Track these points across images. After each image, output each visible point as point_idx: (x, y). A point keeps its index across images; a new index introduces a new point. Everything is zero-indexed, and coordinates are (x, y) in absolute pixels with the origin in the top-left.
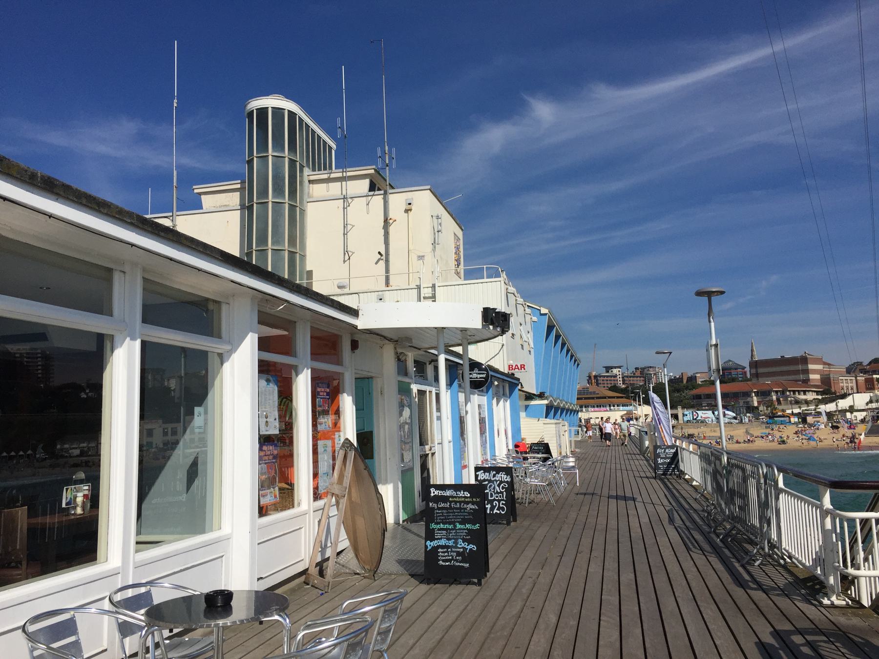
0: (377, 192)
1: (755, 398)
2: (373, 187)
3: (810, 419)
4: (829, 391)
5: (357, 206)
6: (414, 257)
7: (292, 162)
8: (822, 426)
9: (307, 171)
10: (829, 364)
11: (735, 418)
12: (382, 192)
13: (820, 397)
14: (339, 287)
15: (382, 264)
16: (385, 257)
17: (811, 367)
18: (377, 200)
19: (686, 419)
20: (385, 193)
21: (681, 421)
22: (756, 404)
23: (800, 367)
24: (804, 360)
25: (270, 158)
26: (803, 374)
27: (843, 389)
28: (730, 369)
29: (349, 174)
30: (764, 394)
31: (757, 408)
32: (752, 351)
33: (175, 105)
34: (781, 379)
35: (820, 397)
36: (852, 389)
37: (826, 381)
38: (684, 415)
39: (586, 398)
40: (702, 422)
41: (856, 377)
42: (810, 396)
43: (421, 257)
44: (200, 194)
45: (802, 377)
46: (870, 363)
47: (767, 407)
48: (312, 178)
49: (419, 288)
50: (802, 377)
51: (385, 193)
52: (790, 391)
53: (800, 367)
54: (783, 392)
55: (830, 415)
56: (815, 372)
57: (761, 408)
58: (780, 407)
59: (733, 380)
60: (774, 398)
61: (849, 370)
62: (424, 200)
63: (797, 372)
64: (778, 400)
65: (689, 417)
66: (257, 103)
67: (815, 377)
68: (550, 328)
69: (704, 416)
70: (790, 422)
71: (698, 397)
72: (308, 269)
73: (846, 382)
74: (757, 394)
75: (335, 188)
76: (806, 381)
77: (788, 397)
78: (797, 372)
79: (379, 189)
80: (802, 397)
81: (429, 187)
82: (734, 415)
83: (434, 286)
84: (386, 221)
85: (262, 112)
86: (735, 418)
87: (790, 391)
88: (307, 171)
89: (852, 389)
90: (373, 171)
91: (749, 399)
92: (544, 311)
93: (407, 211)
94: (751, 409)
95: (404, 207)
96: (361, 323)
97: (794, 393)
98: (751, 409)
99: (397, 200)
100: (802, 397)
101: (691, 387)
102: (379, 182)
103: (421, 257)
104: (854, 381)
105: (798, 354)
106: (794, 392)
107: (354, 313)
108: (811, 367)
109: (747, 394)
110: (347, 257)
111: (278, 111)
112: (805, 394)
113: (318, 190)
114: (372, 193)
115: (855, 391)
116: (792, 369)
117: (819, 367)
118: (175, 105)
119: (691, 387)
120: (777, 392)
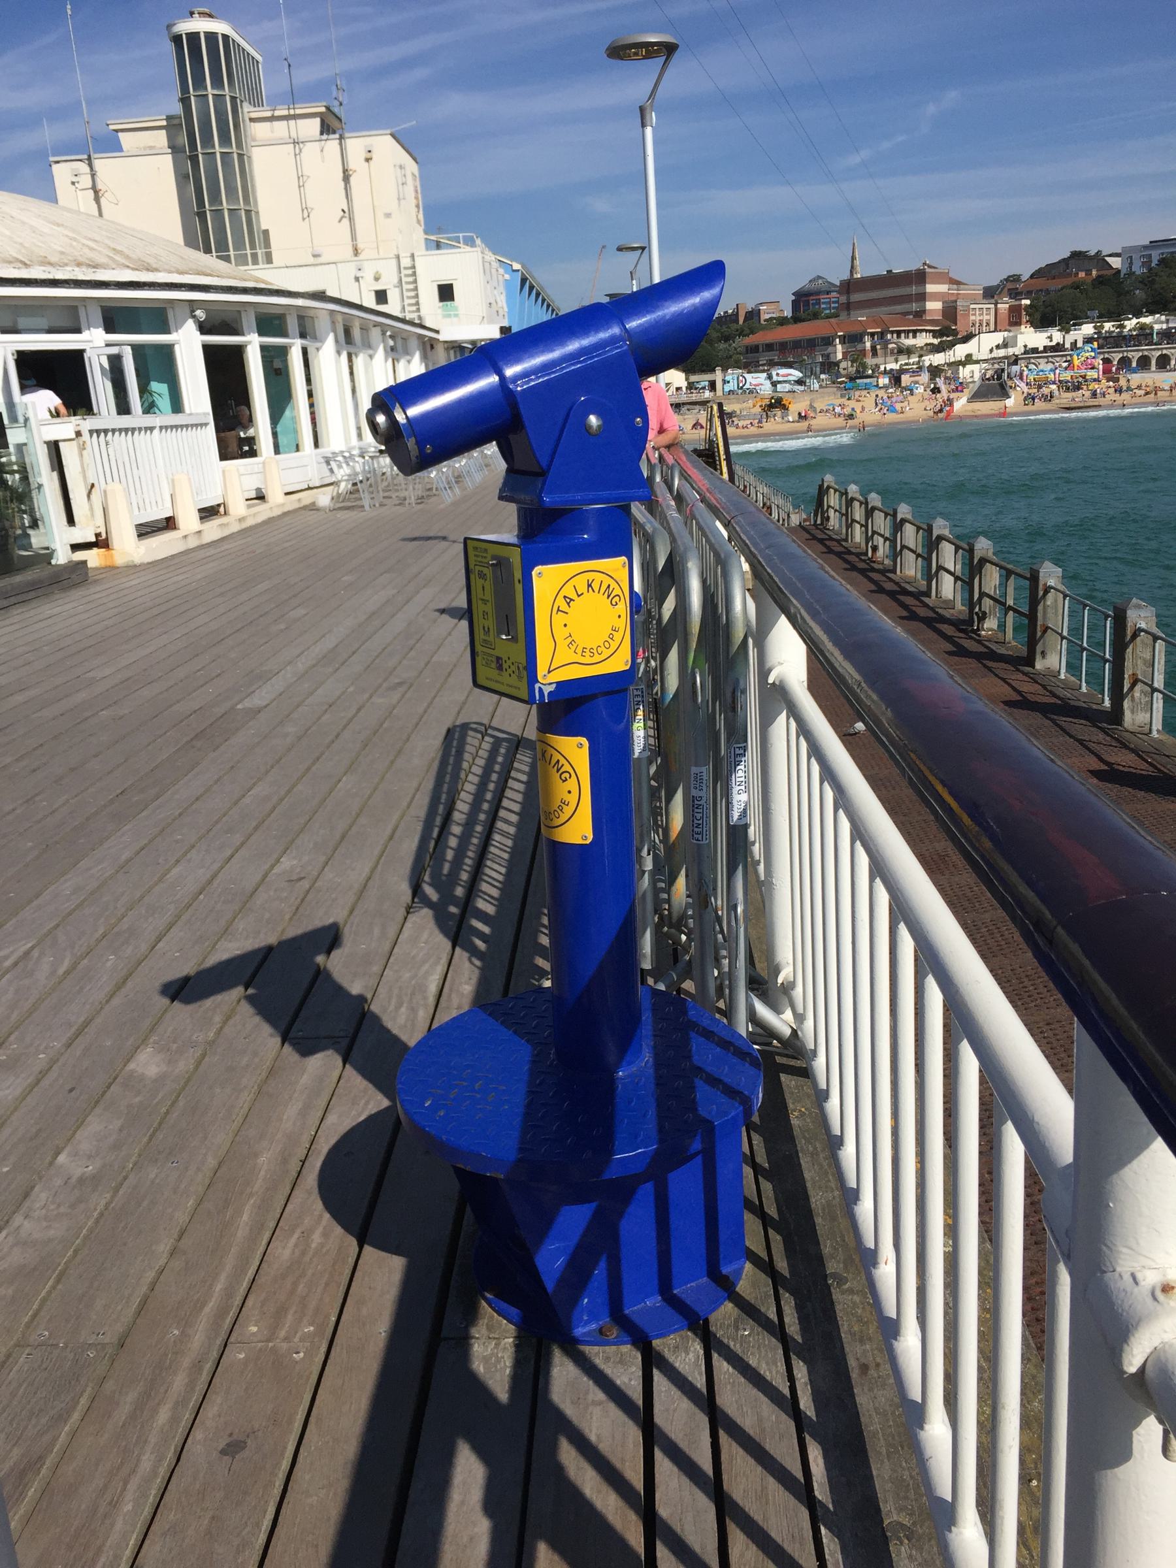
0: (332, 136)
1: (839, 347)
2: (326, 129)
3: (906, 379)
4: (950, 331)
5: (311, 150)
6: (380, 215)
7: (233, 99)
8: (921, 390)
9: (245, 104)
10: (958, 283)
11: (800, 382)
12: (337, 136)
13: (936, 341)
14: (315, 256)
15: (346, 221)
16: (348, 214)
17: (930, 288)
18: (332, 144)
19: (727, 388)
20: (341, 138)
21: (719, 392)
22: (839, 356)
23: (914, 289)
24: (920, 277)
25: (210, 97)
26: (917, 301)
27: (974, 325)
28: (818, 293)
29: (298, 112)
30: (853, 339)
31: (837, 364)
32: (853, 258)
33: (69, 12)
34: (882, 311)
35: (936, 341)
36: (988, 324)
37: (950, 312)
38: (725, 382)
39: (43, 1073)
40: (751, 392)
41: (996, 304)
42: (923, 340)
43: (388, 215)
44: (117, 131)
45: (914, 306)
46: (1032, 277)
47: (853, 362)
48: (254, 115)
49: (398, 257)
50: (914, 306)
51: (341, 138)
52: (892, 332)
53: (914, 289)
54: (882, 335)
55: (935, 371)
56: (936, 297)
57: (843, 365)
58: (874, 361)
59: (816, 316)
60: (868, 345)
61: (990, 293)
62: (385, 146)
63: (908, 299)
64: (874, 349)
65: (732, 386)
66: (186, 26)
67: (934, 306)
68: (524, 280)
69: (754, 382)
70: (877, 386)
71: (754, 349)
72: (264, 227)
73: (982, 312)
74: (843, 340)
75: (280, 129)
76: (920, 314)
77: (888, 342)
78: (908, 299)
79: (334, 132)
80: (909, 342)
81: (389, 132)
82: (801, 375)
83: (413, 256)
84: (345, 171)
85: (193, 37)
86: (800, 382)
87: (892, 332)
88: (245, 104)
89: (988, 324)
90: (323, 109)
91: (830, 349)
92: (516, 266)
93: (368, 160)
94: (830, 366)
95: (364, 155)
96: (442, 337)
97: (899, 337)
98: (830, 366)
99: (356, 145)
100: (909, 342)
101: (747, 331)
102: (334, 123)
103: (388, 215)
104: (993, 312)
105: (913, 266)
106: (899, 333)
107: (437, 332)
108: (930, 288)
109: (828, 341)
110: (306, 214)
111: (211, 37)
112: (915, 337)
113: (259, 131)
114: (325, 137)
115: (992, 329)
116: (900, 290)
117: (943, 288)
118: (69, 12)
119: (747, 331)
120: (872, 335)
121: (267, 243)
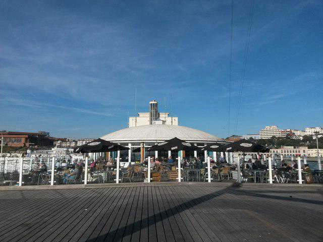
66: (150, 103)
121: (45, 133)
